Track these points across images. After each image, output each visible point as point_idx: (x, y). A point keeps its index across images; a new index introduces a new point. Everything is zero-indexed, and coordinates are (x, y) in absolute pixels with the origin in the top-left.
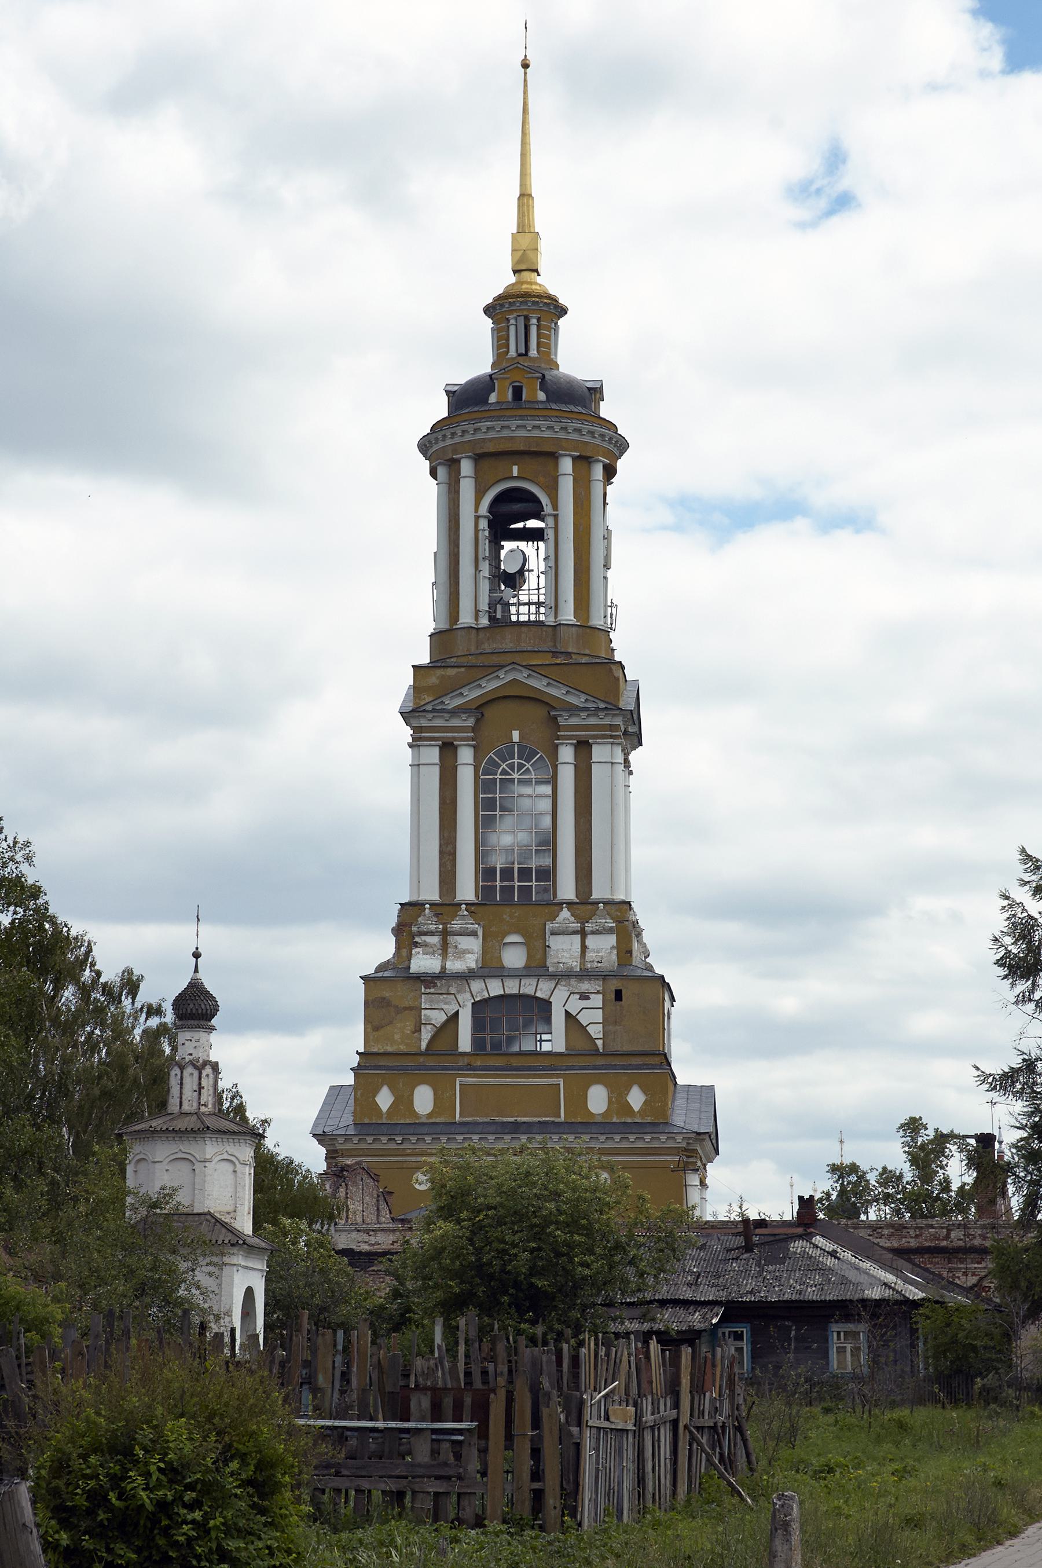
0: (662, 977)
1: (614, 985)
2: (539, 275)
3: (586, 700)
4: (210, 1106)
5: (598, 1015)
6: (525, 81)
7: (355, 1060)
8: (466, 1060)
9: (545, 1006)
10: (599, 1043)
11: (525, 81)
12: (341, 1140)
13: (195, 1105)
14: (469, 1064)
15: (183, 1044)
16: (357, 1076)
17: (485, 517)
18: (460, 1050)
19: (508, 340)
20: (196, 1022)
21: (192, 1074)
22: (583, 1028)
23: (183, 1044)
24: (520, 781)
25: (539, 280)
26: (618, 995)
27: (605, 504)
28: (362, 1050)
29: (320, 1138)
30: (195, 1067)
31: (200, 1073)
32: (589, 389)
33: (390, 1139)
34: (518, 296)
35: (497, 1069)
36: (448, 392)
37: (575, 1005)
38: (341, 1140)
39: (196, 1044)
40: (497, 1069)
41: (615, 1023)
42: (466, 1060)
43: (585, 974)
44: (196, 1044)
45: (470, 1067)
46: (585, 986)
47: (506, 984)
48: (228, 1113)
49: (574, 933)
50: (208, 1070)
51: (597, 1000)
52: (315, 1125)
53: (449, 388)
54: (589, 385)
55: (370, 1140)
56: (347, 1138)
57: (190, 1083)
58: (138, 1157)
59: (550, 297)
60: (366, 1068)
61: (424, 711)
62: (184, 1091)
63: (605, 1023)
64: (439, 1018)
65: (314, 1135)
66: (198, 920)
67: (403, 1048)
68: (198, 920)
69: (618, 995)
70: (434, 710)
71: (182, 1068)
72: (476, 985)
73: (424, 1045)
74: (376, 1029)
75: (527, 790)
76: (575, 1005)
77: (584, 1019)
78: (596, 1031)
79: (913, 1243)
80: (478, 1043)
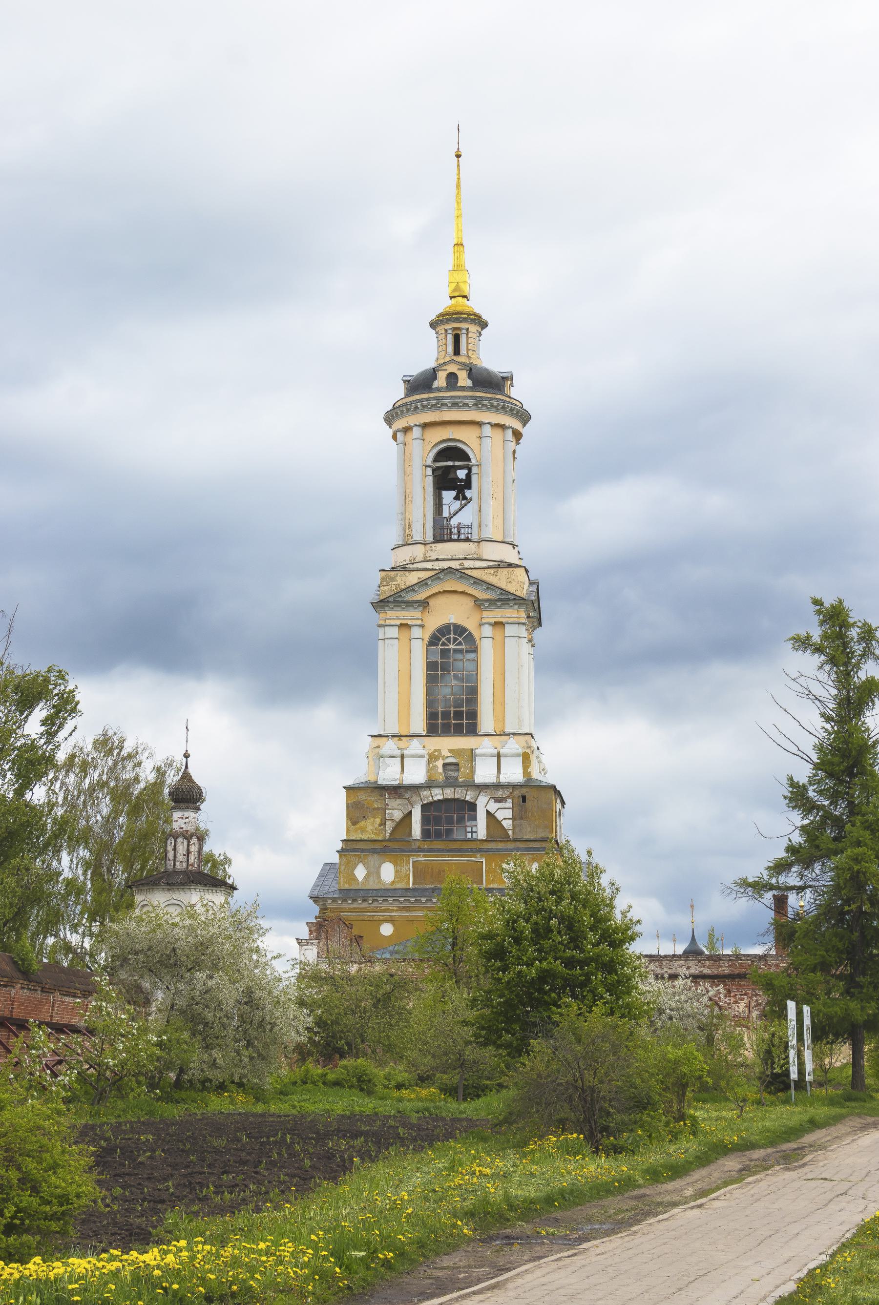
0: (555, 786)
1: (518, 793)
2: (468, 300)
3: (501, 594)
4: (196, 866)
5: (509, 814)
6: (458, 166)
7: (339, 846)
8: (417, 844)
9: (472, 807)
10: (510, 833)
11: (458, 166)
12: (330, 901)
13: (185, 865)
14: (419, 848)
15: (177, 821)
16: (340, 856)
17: (430, 467)
18: (413, 838)
19: (446, 345)
20: (186, 805)
21: (182, 843)
22: (499, 822)
23: (177, 821)
24: (455, 651)
25: (468, 303)
26: (524, 798)
27: (514, 458)
28: (344, 838)
29: (315, 899)
30: (185, 838)
31: (189, 842)
32: (503, 378)
33: (364, 900)
34: (454, 314)
35: (439, 851)
36: (404, 381)
37: (493, 807)
38: (330, 901)
39: (187, 821)
40: (439, 851)
41: (521, 818)
42: (417, 844)
43: (498, 786)
44: (187, 821)
45: (420, 850)
46: (500, 793)
47: (445, 792)
48: (564, 988)
49: (491, 756)
50: (194, 840)
51: (509, 804)
52: (312, 891)
53: (405, 378)
54: (502, 375)
55: (350, 901)
56: (335, 900)
57: (182, 848)
58: (142, 903)
59: (475, 315)
60: (347, 850)
61: (388, 602)
62: (178, 855)
63: (514, 818)
64: (397, 815)
65: (311, 898)
66: (188, 730)
67: (373, 837)
68: (188, 730)
69: (524, 798)
70: (395, 601)
71: (176, 839)
72: (426, 793)
73: (387, 835)
74: (354, 823)
75: (460, 657)
76: (493, 807)
77: (499, 815)
78: (508, 824)
79: (727, 971)
80: (426, 833)
